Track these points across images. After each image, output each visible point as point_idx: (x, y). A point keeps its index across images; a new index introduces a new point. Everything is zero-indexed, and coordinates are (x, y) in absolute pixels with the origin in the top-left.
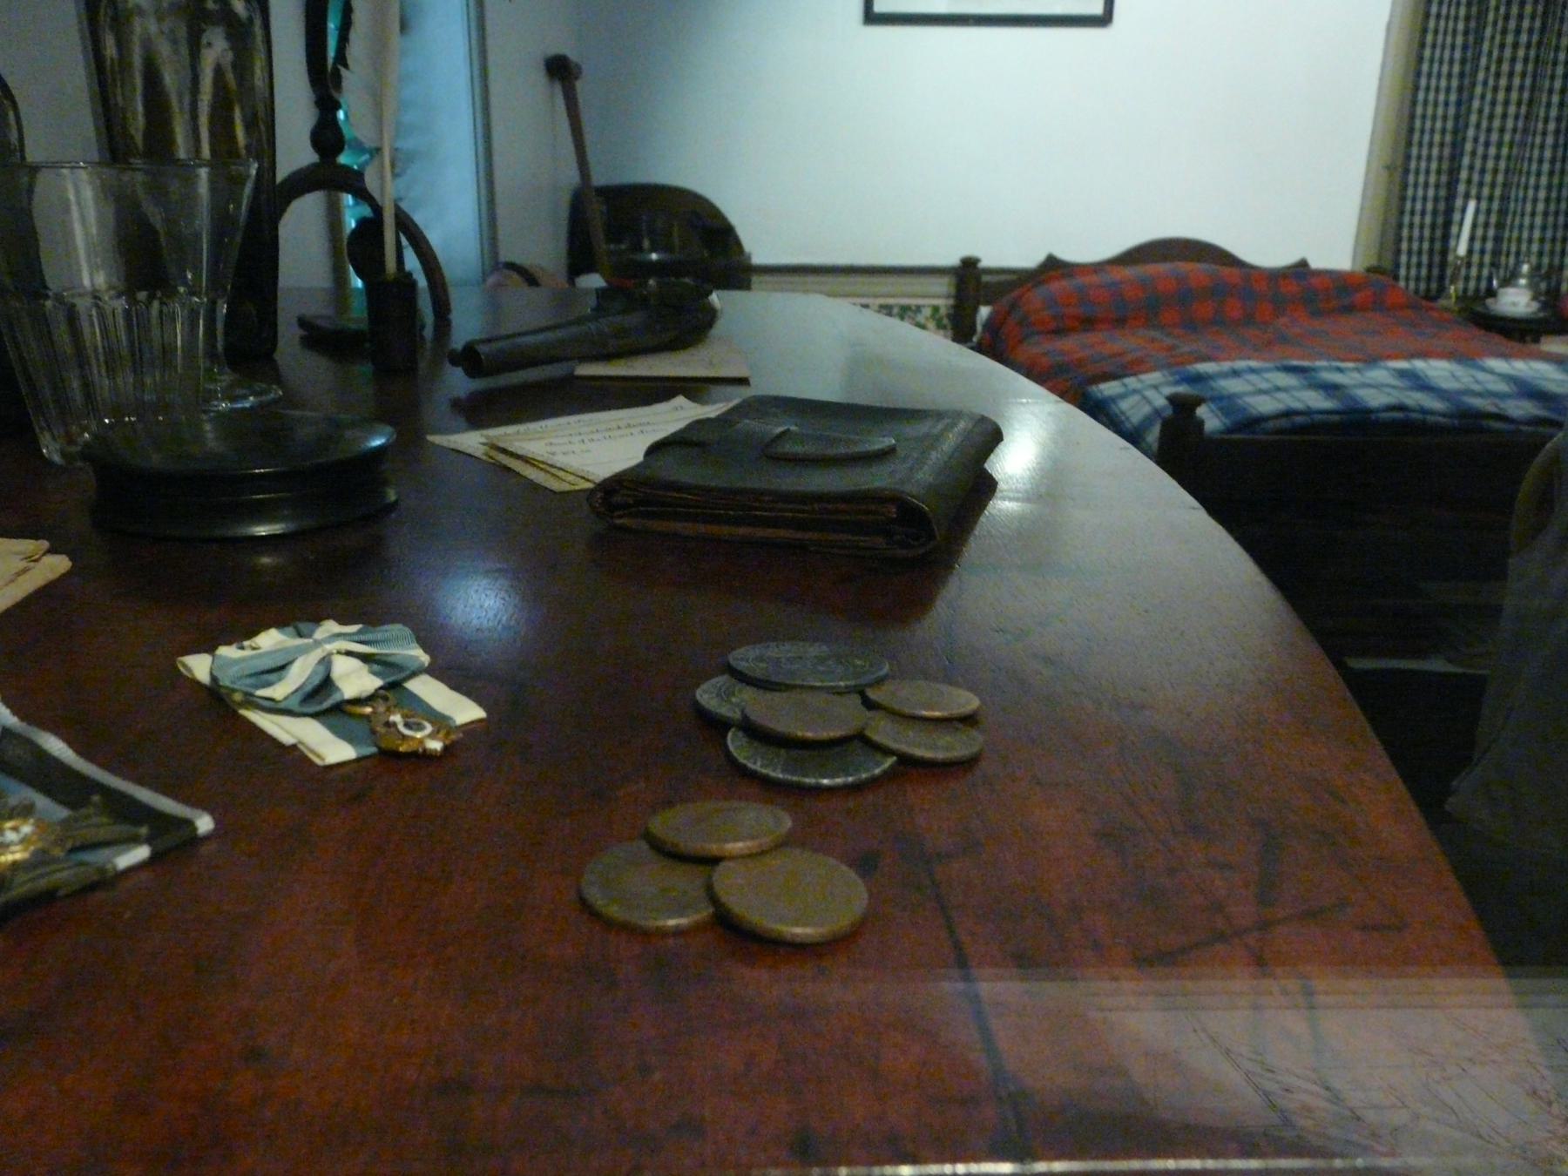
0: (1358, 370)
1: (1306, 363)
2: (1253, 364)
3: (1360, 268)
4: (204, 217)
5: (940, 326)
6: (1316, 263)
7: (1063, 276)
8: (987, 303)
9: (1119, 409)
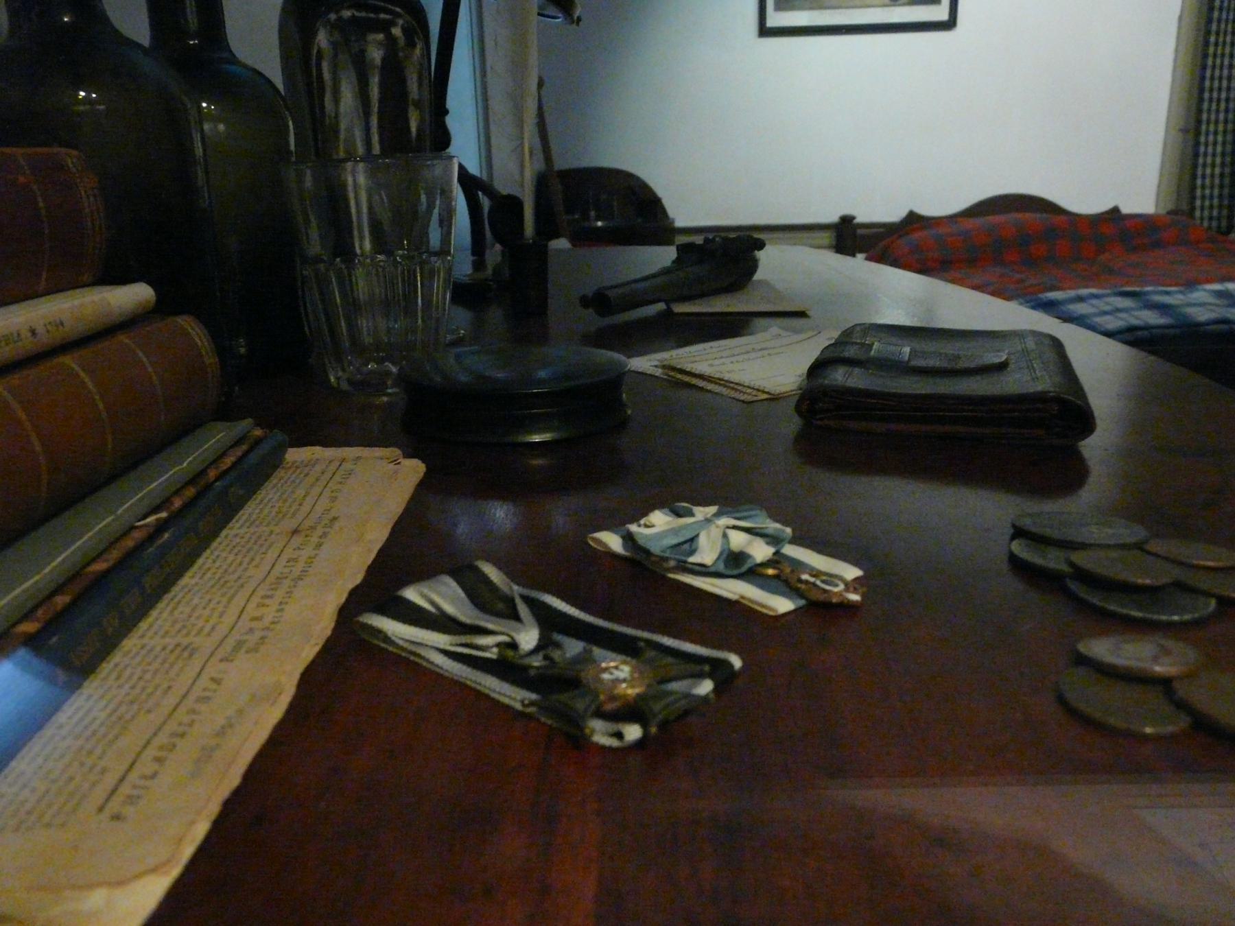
0: (1181, 292)
1: (1138, 289)
2: (1094, 291)
3: (1162, 211)
6: (1126, 209)
7: (922, 228)
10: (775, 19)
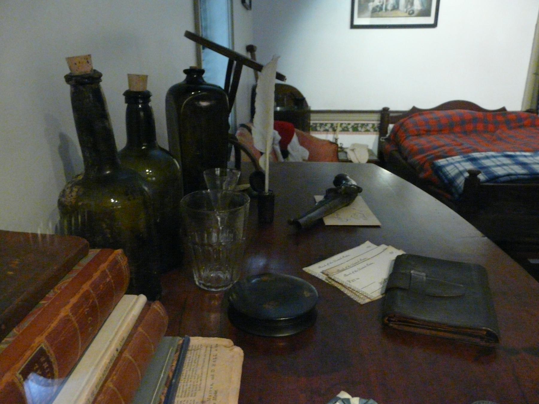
0: (531, 156)
3: (524, 110)
5: (375, 131)
6: (509, 109)
7: (420, 114)
8: (392, 123)
9: (447, 170)
10: (357, 22)
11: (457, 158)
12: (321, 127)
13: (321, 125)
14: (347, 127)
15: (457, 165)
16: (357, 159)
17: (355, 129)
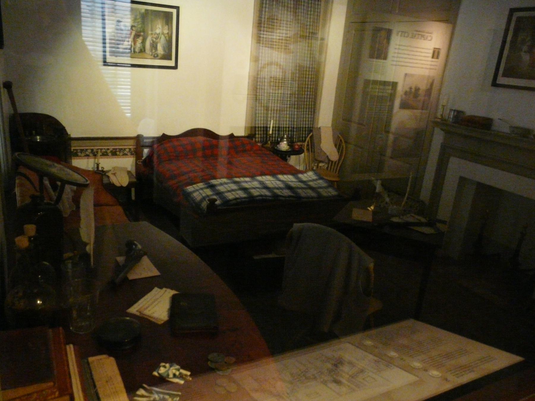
3: (246, 135)
4: (120, 277)
5: (132, 154)
11: (201, 185)
12: (81, 153)
13: (82, 151)
14: (106, 152)
15: (201, 191)
16: (120, 183)
17: (114, 153)
